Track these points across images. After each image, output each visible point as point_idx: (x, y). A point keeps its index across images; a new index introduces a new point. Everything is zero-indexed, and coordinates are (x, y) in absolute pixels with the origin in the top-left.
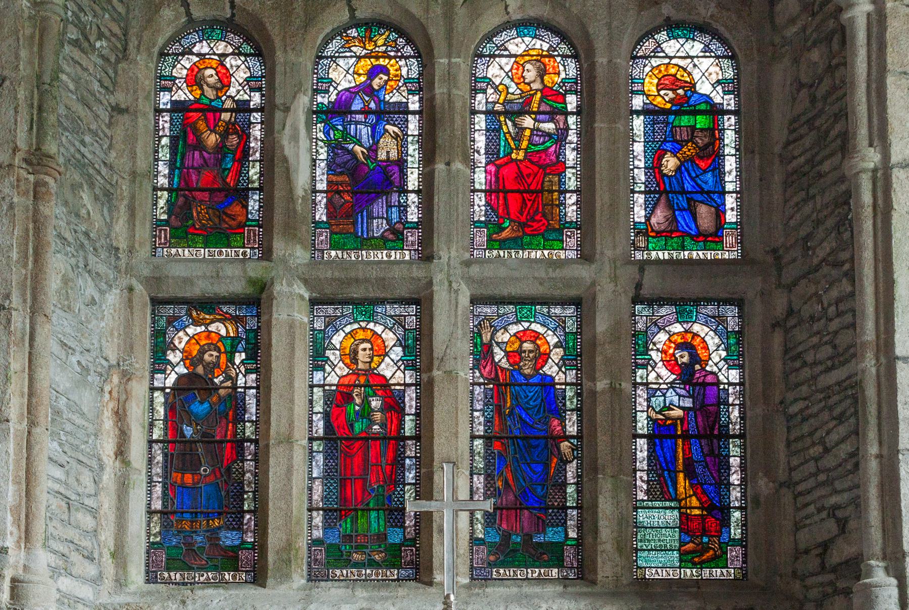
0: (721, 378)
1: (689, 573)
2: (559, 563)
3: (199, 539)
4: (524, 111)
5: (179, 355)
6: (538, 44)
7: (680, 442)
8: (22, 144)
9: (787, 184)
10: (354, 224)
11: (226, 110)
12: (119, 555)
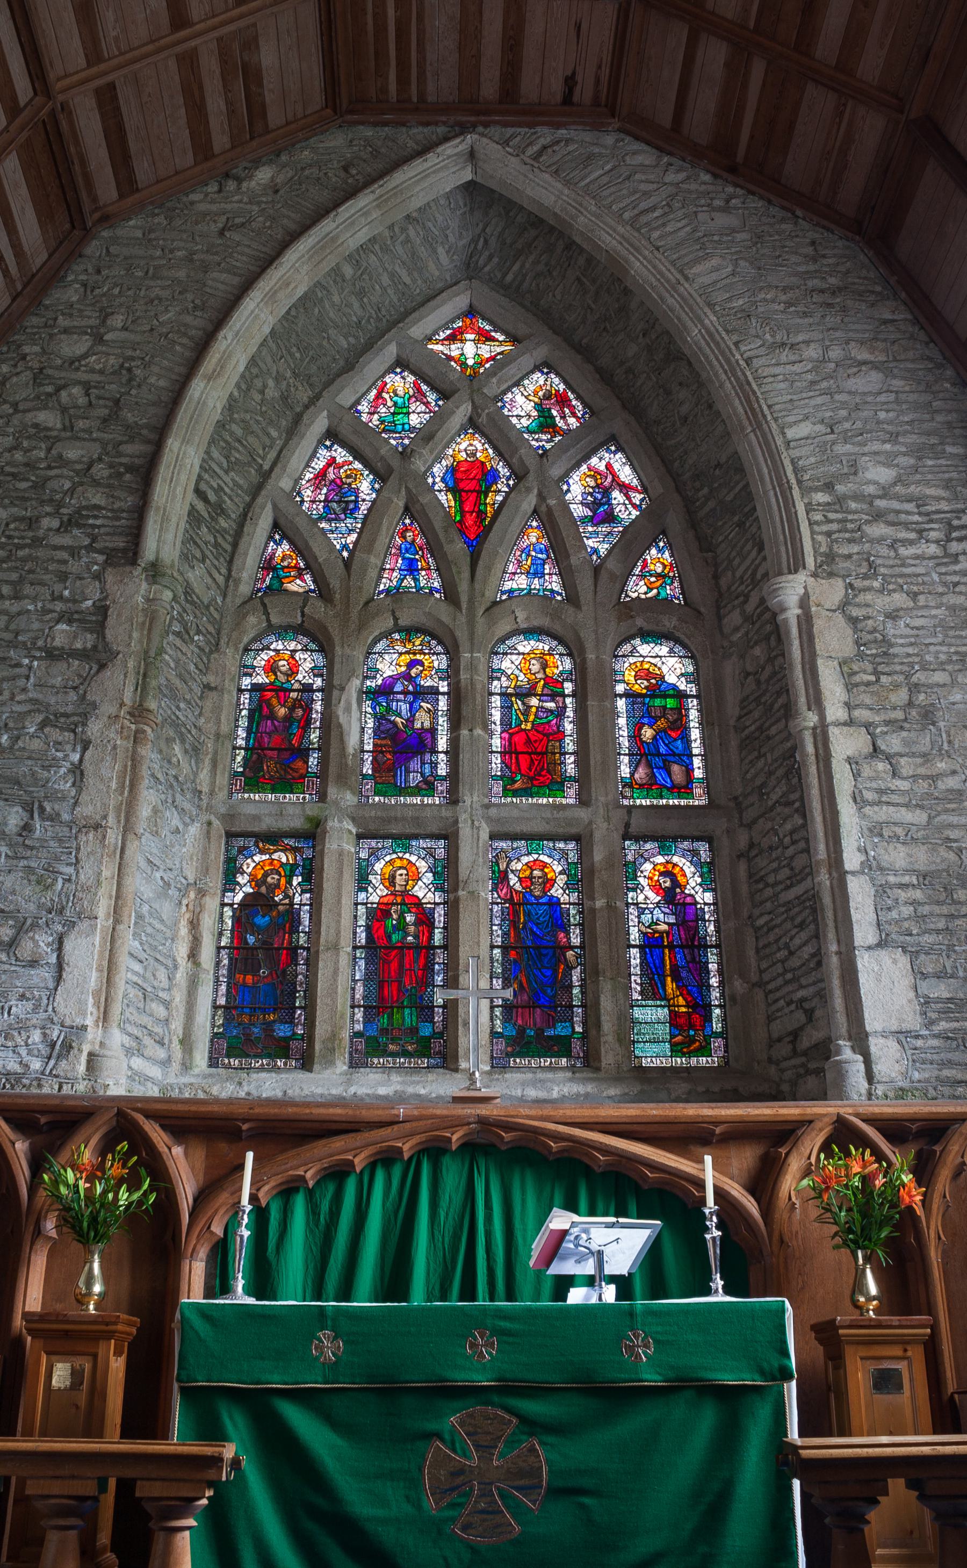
0: (698, 899)
1: (679, 1061)
2: (568, 1054)
3: (256, 1030)
4: (531, 692)
5: (246, 878)
6: (541, 645)
7: (667, 951)
8: (128, 701)
9: (741, 747)
10: (395, 776)
11: (294, 691)
12: (187, 1042)
